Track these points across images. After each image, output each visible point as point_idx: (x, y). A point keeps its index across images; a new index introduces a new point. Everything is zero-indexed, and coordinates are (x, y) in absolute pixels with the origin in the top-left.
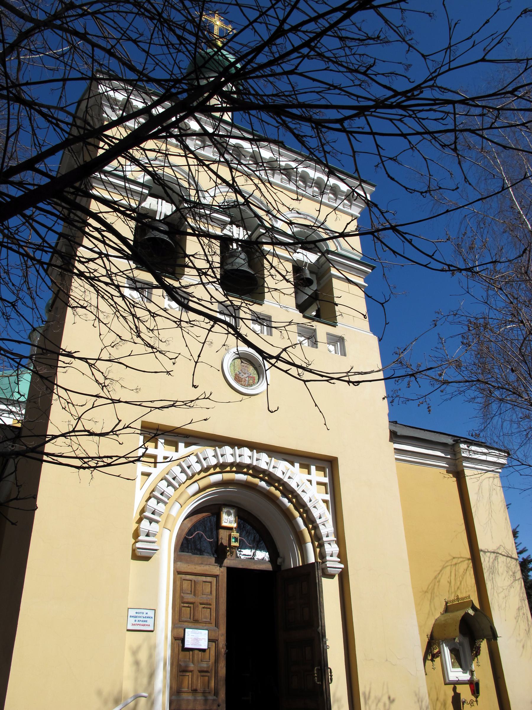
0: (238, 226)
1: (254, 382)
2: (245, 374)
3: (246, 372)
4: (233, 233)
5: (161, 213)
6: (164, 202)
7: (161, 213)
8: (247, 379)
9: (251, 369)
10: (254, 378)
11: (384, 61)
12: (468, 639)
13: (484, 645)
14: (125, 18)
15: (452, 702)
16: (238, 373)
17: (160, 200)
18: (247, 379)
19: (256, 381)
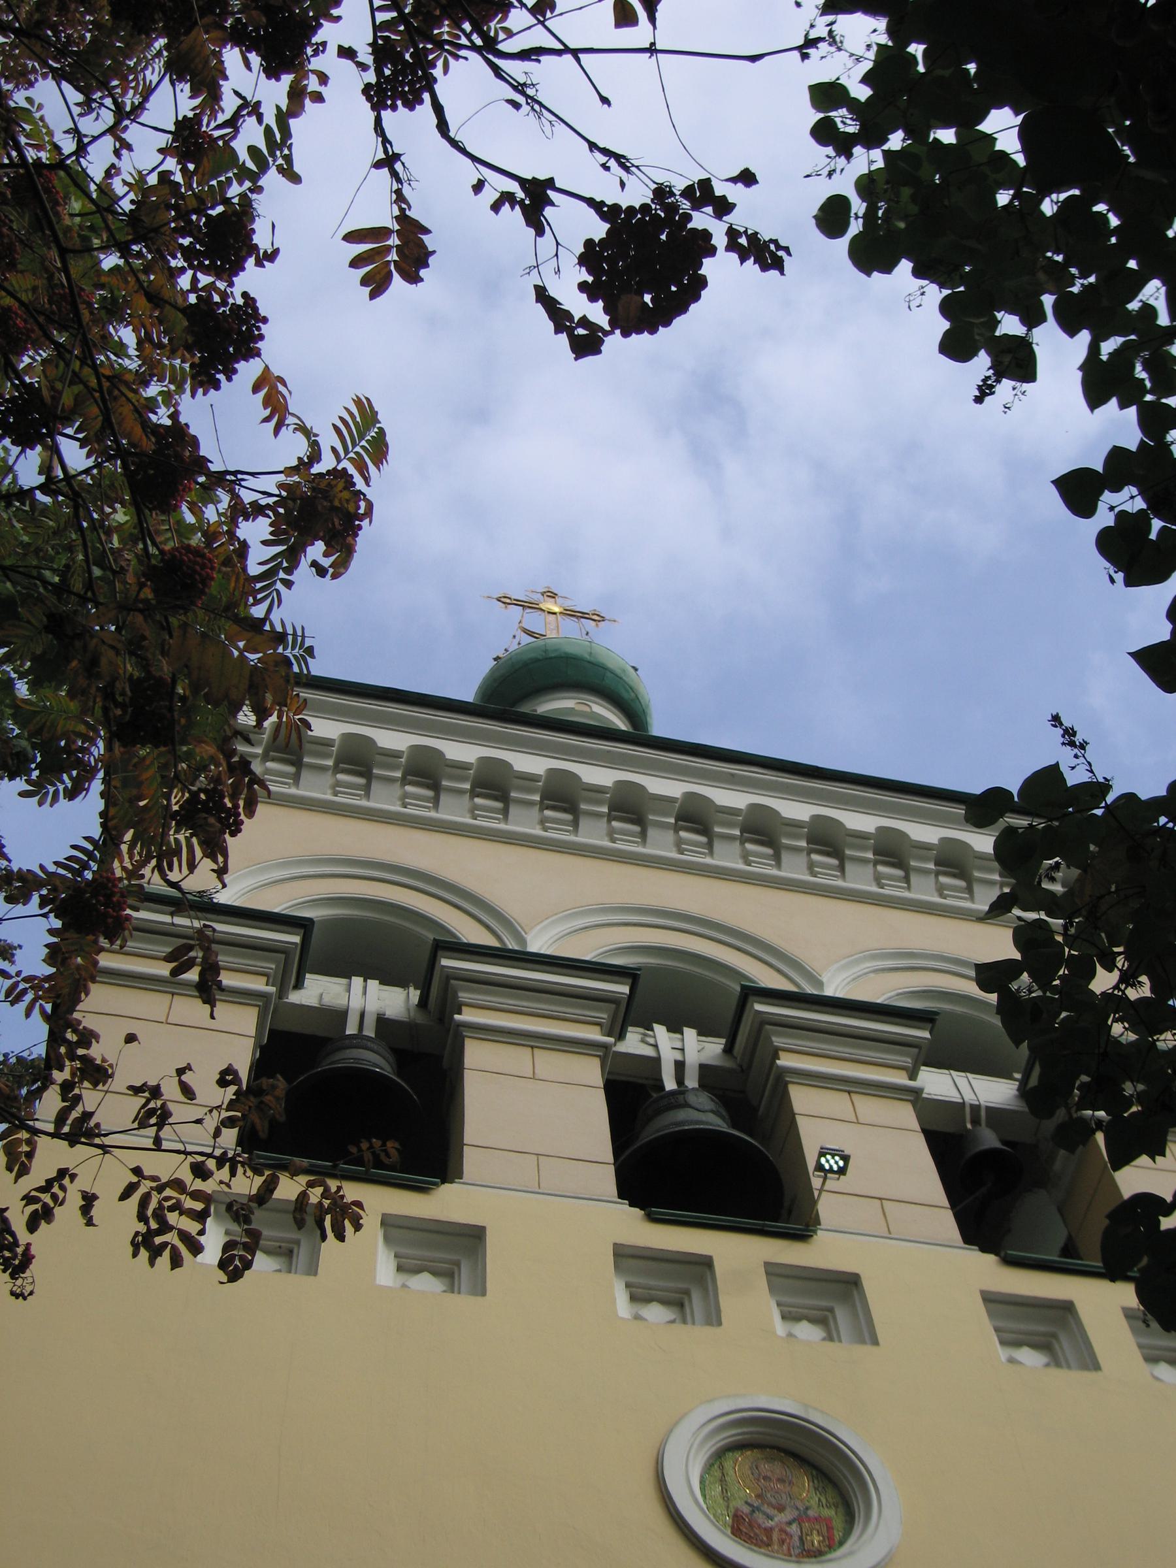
0: (675, 1028)
1: (830, 1538)
2: (781, 1509)
3: (784, 1499)
4: (656, 1046)
5: (362, 1015)
6: (373, 984)
7: (362, 1015)
8: (794, 1529)
9: (806, 1491)
10: (828, 1522)
11: (754, 59)
12: (1165, 793)
13: (426, 96)
14: (652, 50)
15: (653, 331)
16: (746, 1509)
17: (357, 981)
18: (794, 1529)
19: (838, 1535)
